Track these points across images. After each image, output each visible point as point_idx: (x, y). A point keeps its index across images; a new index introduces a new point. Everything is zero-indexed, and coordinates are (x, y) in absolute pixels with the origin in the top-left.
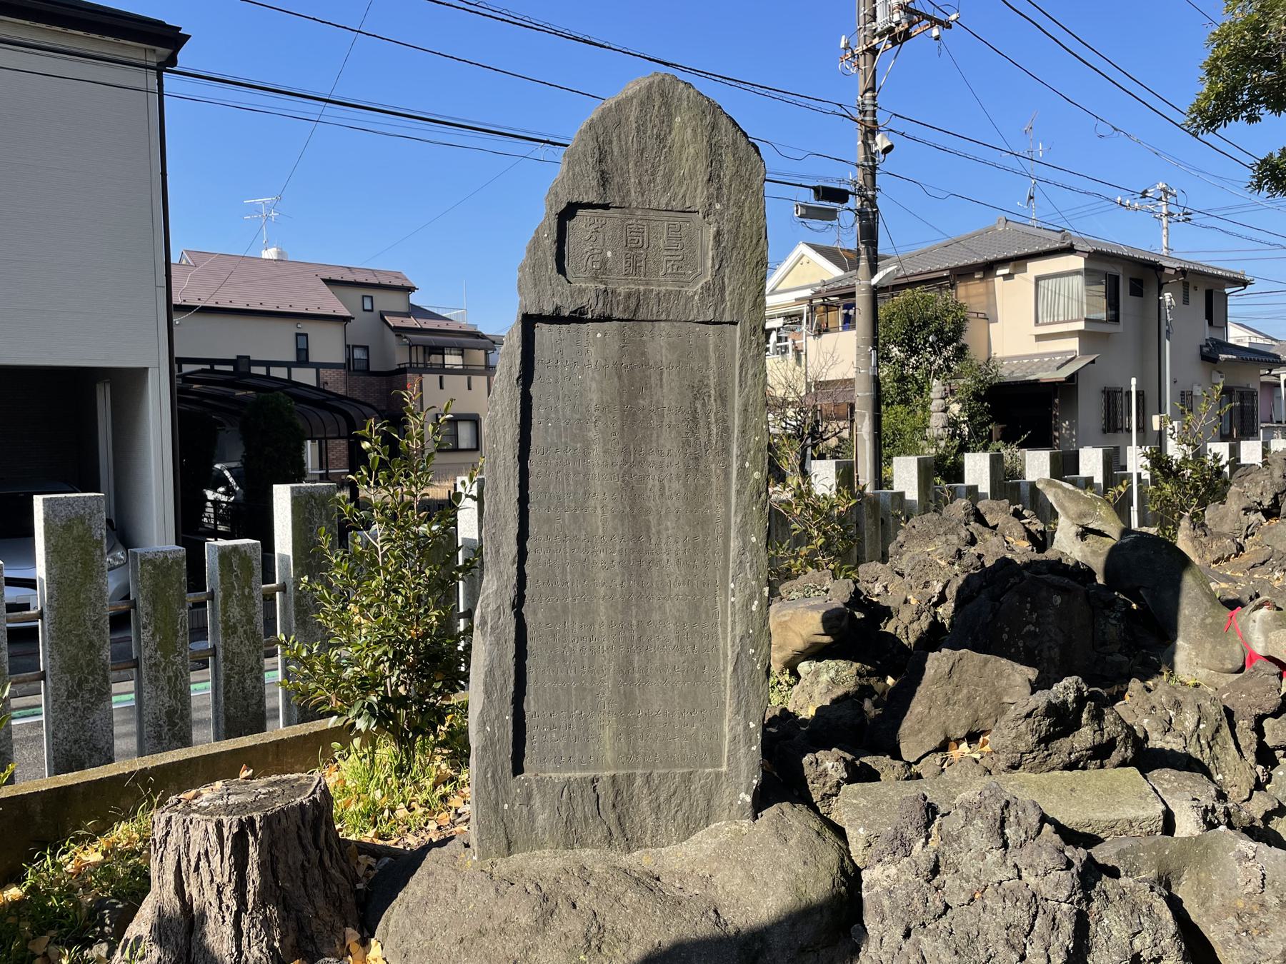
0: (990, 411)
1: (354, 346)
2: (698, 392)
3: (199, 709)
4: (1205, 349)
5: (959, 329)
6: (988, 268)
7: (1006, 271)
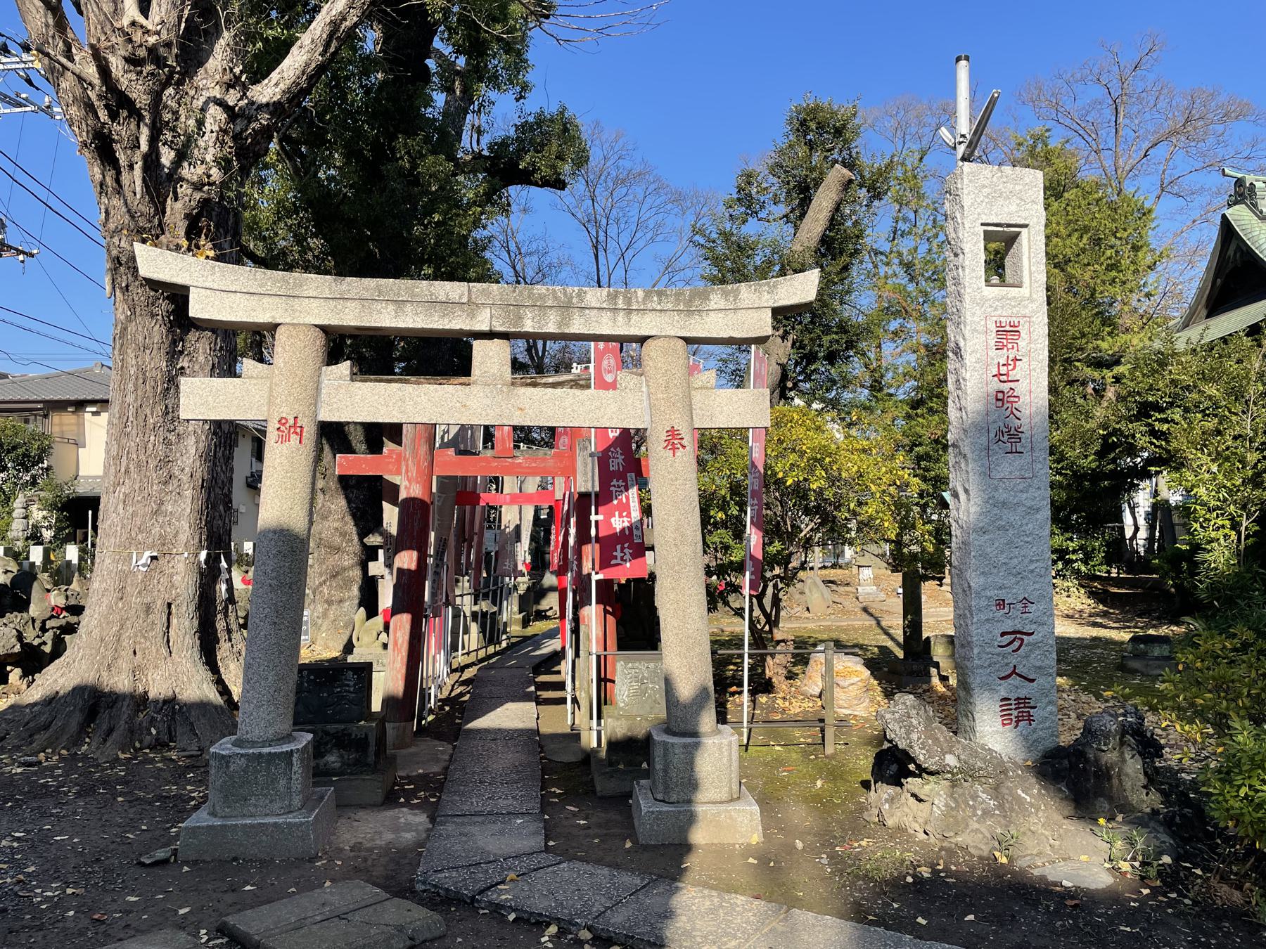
0: (67, 519)
3: (593, 486)
4: (250, 480)
5: (44, 452)
6: (80, 405)
7: (94, 409)
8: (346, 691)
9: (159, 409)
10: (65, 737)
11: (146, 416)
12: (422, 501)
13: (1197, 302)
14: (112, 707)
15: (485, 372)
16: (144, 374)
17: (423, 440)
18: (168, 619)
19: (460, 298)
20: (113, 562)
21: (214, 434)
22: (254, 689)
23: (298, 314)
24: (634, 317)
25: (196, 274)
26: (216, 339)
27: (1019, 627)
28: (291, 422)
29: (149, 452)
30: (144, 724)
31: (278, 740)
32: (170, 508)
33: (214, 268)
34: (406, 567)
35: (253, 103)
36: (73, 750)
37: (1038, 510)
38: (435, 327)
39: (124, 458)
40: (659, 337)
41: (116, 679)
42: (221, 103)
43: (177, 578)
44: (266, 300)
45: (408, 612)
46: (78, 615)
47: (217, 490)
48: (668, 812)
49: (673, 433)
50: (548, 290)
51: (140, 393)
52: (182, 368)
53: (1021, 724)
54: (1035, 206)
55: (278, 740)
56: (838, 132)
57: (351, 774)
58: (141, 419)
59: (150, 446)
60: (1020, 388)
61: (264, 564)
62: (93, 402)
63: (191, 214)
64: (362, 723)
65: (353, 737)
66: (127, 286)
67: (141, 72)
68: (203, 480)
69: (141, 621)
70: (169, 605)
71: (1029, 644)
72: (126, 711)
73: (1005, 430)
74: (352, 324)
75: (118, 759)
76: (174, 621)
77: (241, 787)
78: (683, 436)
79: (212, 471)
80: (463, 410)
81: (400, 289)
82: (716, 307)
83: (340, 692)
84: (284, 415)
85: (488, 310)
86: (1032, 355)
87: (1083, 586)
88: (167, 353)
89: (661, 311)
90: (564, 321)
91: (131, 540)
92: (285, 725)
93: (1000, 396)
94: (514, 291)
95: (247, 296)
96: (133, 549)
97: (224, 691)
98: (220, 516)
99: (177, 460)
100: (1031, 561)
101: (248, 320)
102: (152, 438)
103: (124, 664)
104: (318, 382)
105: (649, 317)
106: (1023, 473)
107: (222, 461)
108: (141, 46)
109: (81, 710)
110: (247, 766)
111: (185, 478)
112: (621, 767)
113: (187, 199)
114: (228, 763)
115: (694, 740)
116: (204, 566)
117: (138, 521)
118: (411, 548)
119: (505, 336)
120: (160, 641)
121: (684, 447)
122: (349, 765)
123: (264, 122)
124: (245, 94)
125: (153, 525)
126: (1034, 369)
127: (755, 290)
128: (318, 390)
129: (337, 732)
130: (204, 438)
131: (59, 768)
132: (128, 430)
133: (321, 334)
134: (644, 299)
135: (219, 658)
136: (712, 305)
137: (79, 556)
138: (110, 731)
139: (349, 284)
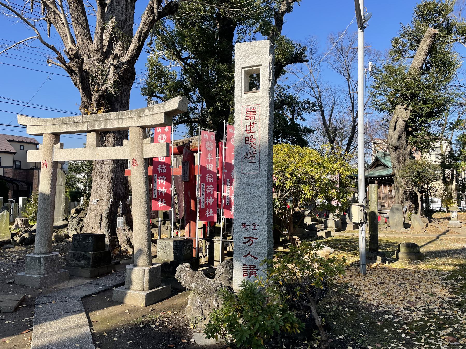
1: (16, 161)
2: (60, 190)
24: (124, 121)
26: (115, 135)
27: (251, 235)
28: (44, 162)
32: (103, 186)
35: (121, 62)
37: (261, 186)
42: (113, 64)
43: (104, 207)
44: (41, 127)
53: (252, 276)
54: (265, 56)
57: (86, 268)
60: (256, 135)
63: (97, 100)
67: (74, 62)
71: (255, 243)
73: (249, 153)
78: (137, 161)
85: (87, 123)
86: (261, 120)
89: (131, 118)
93: (247, 139)
100: (257, 208)
105: (128, 120)
106: (255, 171)
108: (71, 54)
113: (95, 96)
121: (137, 165)
123: (125, 68)
124: (119, 60)
126: (262, 126)
134: (127, 114)
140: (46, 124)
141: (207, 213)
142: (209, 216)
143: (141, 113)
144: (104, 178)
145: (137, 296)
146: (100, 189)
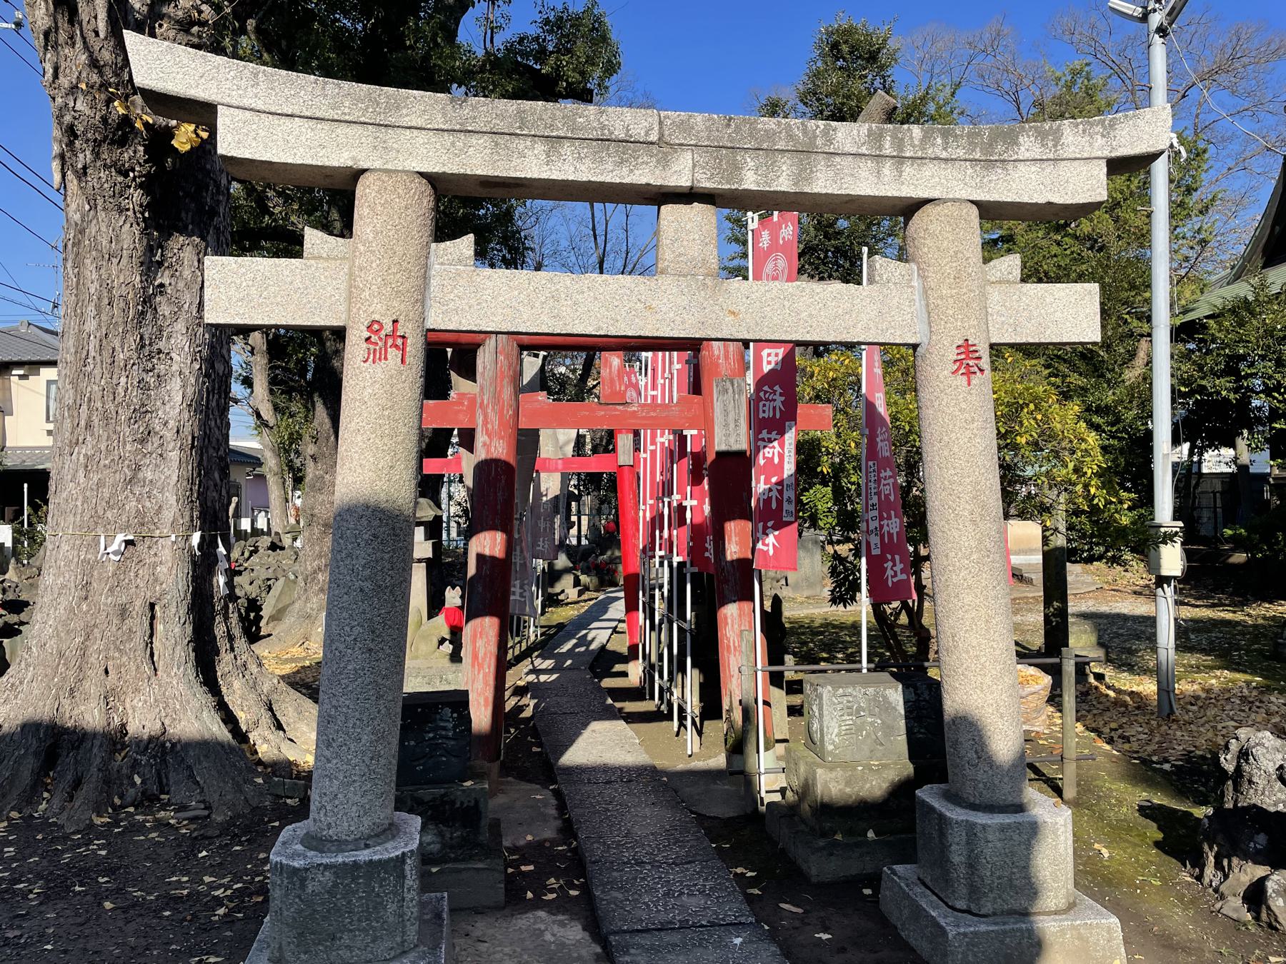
7: (21, 372)
8: (442, 737)
9: (132, 341)
10: (15, 793)
11: (114, 349)
12: (506, 463)
13: (1253, 253)
14: (78, 748)
15: (680, 255)
16: (110, 291)
17: (505, 382)
18: (151, 625)
19: (647, 134)
20: (73, 548)
21: (205, 376)
22: (338, 756)
23: (393, 154)
24: (908, 169)
25: (229, 84)
28: (388, 328)
29: (119, 399)
30: (124, 771)
31: (377, 835)
32: (149, 476)
33: (256, 75)
34: (487, 552)
36: (27, 811)
38: (608, 179)
39: (85, 407)
40: (945, 201)
41: (83, 708)
43: (162, 570)
44: (342, 130)
45: (491, 614)
46: (18, 614)
47: (211, 451)
48: (988, 932)
49: (967, 349)
50: (779, 124)
51: (104, 318)
52: (162, 285)
55: (377, 835)
56: (873, 57)
57: (456, 860)
58: (106, 354)
59: (120, 390)
61: (349, 555)
62: (20, 364)
64: (468, 783)
65: (458, 805)
66: (85, 168)
68: (193, 438)
69: (114, 629)
70: (152, 606)
72: (98, 755)
74: (479, 172)
75: (91, 826)
76: (159, 627)
77: (325, 918)
79: (204, 425)
80: (647, 313)
81: (553, 118)
82: (1027, 155)
83: (434, 738)
84: (377, 317)
85: (689, 153)
87: (1142, 561)
88: (142, 264)
89: (946, 160)
90: (803, 173)
91: (97, 519)
92: (384, 812)
94: (728, 126)
95: (312, 123)
96: (100, 531)
97: (229, 719)
98: (216, 485)
99: (157, 410)
101: (314, 163)
102: (123, 380)
103: (93, 686)
104: (426, 267)
105: (930, 170)
107: (216, 413)
109: (36, 754)
110: (335, 885)
111: (169, 435)
112: (839, 837)
114: (303, 881)
115: (1017, 818)
116: (198, 553)
117: (106, 492)
118: (493, 528)
119: (708, 197)
120: (141, 654)
121: (982, 371)
122: (452, 847)
125: (127, 498)
127: (1084, 131)
128: (425, 278)
129: (434, 800)
130: (193, 380)
131: (10, 844)
132: (89, 369)
133: (428, 190)
135: (219, 674)
136: (1023, 153)
137: (13, 538)
138: (77, 784)
139: (474, 108)
140: (391, 120)
141: (889, 573)
142: (895, 580)
143: (1000, 148)
144: (156, 440)
145: (1080, 937)
146: (137, 490)
